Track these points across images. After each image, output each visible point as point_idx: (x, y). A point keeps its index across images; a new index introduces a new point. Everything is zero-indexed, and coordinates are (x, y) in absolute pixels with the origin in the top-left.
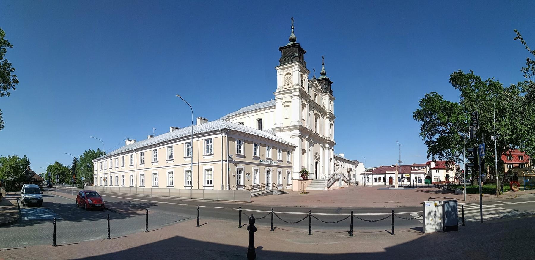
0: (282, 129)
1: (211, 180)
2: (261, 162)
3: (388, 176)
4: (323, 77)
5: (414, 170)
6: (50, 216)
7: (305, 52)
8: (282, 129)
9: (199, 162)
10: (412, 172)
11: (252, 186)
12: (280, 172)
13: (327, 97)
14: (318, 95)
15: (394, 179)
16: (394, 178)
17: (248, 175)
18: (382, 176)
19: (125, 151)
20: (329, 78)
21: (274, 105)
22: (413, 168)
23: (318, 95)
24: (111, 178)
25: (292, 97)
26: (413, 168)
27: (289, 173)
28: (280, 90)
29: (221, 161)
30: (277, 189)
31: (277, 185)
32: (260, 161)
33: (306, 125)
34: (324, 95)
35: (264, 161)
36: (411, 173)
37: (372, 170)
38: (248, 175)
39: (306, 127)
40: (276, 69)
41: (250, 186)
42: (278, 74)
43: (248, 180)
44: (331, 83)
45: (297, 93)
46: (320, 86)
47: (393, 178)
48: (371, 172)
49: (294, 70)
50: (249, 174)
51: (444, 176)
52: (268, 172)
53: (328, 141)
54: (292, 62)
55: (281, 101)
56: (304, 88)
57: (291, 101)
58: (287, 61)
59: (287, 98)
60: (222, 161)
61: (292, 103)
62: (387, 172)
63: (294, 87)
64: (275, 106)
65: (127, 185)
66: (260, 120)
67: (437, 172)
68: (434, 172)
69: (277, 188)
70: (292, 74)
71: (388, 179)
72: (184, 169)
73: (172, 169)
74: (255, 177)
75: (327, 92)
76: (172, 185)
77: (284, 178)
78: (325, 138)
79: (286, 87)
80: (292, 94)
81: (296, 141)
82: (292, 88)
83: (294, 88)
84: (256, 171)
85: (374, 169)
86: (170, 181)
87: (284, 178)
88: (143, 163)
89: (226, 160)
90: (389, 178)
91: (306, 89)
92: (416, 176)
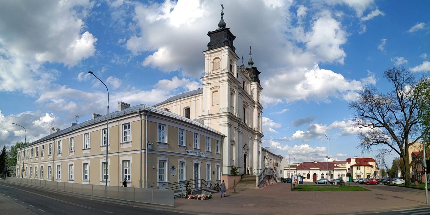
0: (210, 116)
1: (129, 174)
2: (188, 152)
3: (312, 173)
4: (250, 67)
5: (337, 167)
6: (283, 138)
7: (235, 38)
8: (210, 116)
9: (119, 151)
10: (335, 169)
11: (178, 183)
12: (208, 166)
13: (255, 86)
14: (247, 83)
15: (318, 176)
16: (318, 174)
17: (173, 168)
18: (307, 172)
19: (48, 139)
20: (257, 68)
21: (202, 92)
22: (335, 165)
23: (247, 83)
24: (42, 168)
25: (220, 82)
26: (335, 165)
27: (218, 166)
28: (208, 75)
29: (139, 150)
30: (206, 187)
31: (206, 182)
32: (187, 152)
33: (235, 112)
34: (252, 85)
35: (192, 152)
36: (333, 170)
37: (297, 166)
38: (173, 168)
39: (235, 115)
40: (204, 54)
41: (175, 183)
42: (206, 59)
43: (173, 175)
44: (259, 73)
45: (226, 78)
46: (248, 74)
47: (317, 175)
48: (296, 168)
49: (223, 54)
50: (174, 168)
51: (365, 174)
52: (196, 165)
53: (256, 133)
54: (221, 47)
55: (209, 86)
56: (233, 73)
57: (219, 87)
58: (215, 46)
59: (215, 82)
60: (140, 150)
61: (224, 180)
62: (311, 168)
63: (223, 72)
64: (203, 93)
65: (45, 178)
66: (187, 109)
67: (358, 169)
68: (355, 169)
69: (206, 185)
70: (220, 59)
71: (312, 176)
72: (57, 164)
73: (60, 163)
74: (181, 171)
75: (255, 81)
76: (87, 179)
77: (214, 173)
78: (254, 129)
79: (214, 72)
80: (221, 79)
81: (224, 130)
82: (221, 73)
83: (223, 73)
84: (182, 163)
85: (298, 165)
86: (124, 169)
87: (214, 173)
88: (60, 153)
89: (145, 149)
90: (313, 175)
91: (235, 76)
92: (339, 173)
